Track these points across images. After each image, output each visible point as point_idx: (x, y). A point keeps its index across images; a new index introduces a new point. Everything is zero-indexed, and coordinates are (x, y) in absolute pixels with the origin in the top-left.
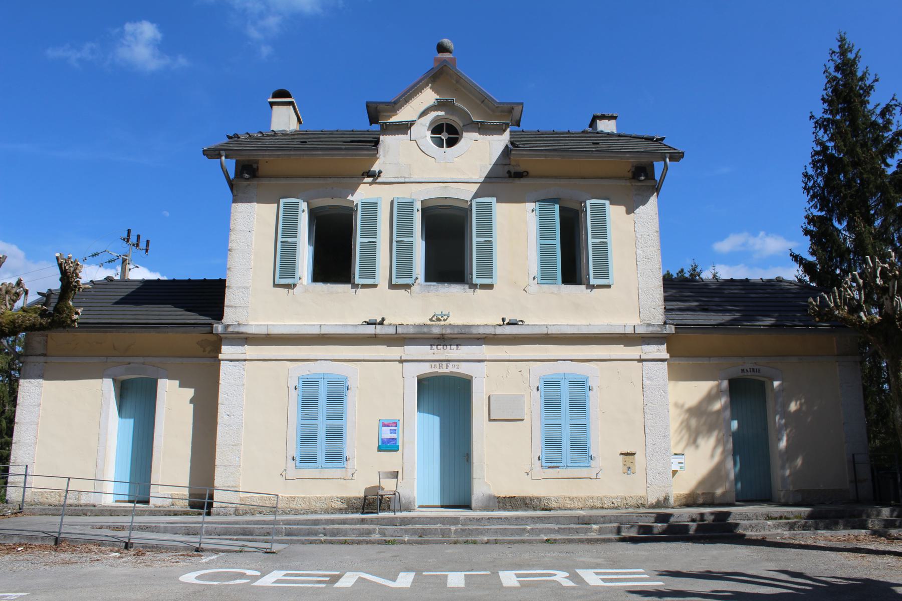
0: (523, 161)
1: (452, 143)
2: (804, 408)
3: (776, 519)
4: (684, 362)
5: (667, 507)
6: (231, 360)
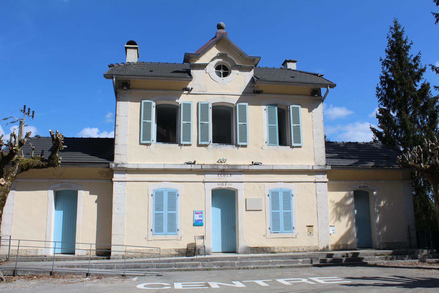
0: (260, 86)
1: (226, 75)
2: (387, 204)
3: (379, 255)
4: (333, 183)
5: (328, 251)
6: (119, 181)
